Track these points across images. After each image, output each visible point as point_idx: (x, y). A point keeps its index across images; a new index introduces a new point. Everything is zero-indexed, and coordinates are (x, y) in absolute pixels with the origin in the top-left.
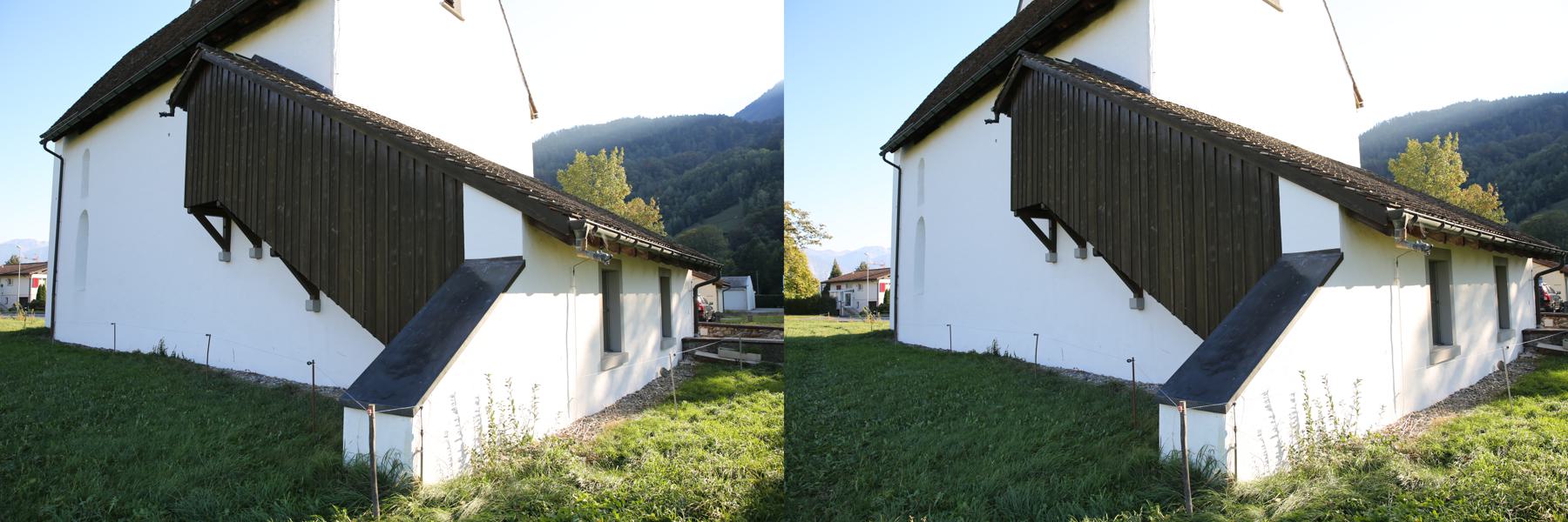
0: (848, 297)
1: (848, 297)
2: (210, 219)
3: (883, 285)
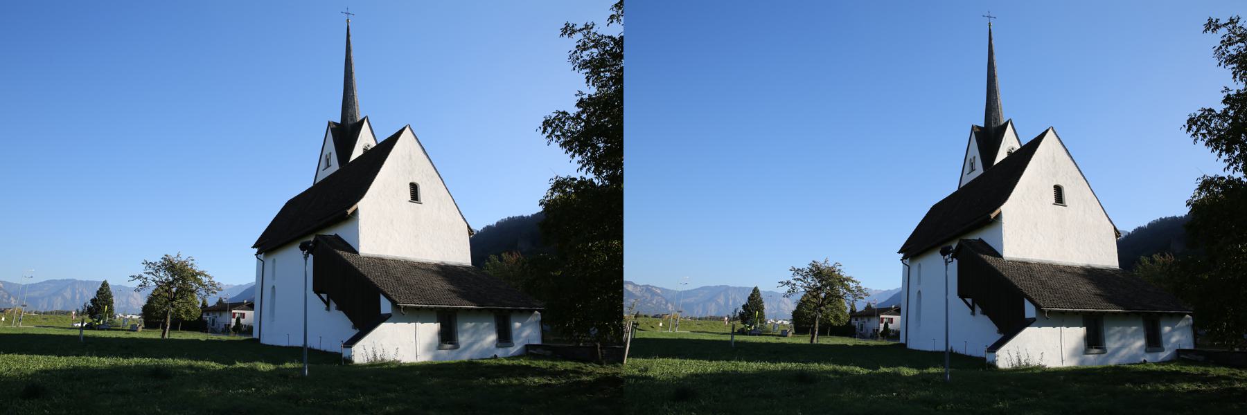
0: (862, 325)
1: (862, 325)
2: (966, 299)
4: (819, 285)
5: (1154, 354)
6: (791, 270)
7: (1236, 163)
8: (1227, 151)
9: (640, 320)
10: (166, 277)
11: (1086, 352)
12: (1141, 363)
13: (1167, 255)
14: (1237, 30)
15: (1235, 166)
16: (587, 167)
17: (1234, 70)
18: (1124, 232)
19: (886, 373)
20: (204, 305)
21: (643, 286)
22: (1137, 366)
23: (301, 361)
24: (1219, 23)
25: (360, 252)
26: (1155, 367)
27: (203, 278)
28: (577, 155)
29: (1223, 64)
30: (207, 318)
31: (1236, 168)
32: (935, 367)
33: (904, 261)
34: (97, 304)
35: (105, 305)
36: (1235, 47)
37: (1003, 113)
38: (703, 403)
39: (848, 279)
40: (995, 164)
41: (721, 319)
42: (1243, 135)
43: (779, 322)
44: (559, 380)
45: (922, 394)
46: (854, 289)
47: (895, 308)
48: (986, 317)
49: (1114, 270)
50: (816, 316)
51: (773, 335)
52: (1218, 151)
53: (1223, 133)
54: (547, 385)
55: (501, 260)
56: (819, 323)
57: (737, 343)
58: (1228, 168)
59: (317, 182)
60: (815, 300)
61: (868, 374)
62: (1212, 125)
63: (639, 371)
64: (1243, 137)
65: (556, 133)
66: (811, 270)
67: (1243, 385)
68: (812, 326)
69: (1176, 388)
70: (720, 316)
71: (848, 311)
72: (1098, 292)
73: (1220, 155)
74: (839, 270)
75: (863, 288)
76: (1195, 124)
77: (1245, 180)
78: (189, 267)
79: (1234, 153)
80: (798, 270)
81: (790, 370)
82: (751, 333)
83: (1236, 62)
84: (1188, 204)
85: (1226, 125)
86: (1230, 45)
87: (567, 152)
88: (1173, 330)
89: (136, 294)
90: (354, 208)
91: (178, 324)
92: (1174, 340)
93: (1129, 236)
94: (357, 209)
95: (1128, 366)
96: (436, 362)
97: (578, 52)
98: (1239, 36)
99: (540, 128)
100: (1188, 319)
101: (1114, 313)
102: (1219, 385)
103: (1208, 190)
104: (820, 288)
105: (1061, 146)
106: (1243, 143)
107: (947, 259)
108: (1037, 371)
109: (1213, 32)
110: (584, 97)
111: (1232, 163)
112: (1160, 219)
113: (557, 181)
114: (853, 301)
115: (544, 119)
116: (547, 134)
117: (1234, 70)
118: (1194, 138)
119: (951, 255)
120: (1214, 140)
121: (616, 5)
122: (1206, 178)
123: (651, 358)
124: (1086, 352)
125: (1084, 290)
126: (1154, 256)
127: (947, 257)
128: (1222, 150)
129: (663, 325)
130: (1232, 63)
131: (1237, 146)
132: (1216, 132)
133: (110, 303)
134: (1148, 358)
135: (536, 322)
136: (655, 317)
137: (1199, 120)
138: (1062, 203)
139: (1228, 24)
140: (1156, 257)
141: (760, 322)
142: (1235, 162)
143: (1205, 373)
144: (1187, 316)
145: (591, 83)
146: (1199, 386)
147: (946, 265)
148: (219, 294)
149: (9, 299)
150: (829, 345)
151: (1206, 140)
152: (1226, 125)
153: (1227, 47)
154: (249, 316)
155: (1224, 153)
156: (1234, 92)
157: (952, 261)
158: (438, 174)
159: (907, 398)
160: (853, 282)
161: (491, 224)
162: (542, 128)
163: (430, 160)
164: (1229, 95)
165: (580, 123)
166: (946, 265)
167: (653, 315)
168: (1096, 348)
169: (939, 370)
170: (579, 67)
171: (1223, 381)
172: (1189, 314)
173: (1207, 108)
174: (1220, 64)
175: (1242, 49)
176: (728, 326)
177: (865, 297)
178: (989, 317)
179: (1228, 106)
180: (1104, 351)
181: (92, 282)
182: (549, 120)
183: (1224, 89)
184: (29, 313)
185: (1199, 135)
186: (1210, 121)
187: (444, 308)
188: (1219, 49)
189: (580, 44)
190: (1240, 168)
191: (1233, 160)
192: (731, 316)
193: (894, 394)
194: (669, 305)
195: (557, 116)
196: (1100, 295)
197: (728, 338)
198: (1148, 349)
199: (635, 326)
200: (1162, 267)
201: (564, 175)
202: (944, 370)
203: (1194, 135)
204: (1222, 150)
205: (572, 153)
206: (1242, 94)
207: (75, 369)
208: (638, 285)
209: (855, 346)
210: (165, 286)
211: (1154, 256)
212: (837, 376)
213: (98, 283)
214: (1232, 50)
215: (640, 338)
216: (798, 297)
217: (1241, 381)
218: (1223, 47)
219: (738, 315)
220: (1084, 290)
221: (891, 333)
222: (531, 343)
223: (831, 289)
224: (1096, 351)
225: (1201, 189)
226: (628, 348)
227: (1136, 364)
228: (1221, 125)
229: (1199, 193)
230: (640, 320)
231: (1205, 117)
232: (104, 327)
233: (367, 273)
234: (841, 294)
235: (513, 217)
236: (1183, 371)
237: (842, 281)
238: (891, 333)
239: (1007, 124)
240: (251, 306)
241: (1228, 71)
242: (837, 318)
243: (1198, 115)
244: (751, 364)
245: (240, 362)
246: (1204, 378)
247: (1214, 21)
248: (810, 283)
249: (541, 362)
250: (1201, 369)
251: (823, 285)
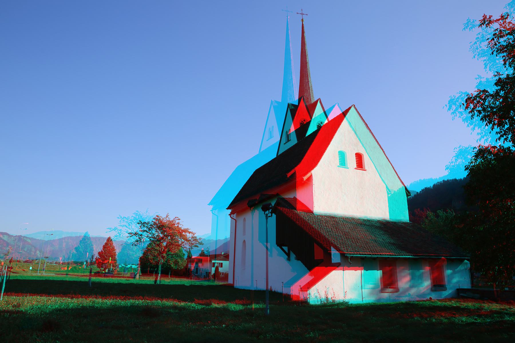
2: (283, 247)
3: (214, 263)
4: (161, 235)
5: (438, 293)
6: (139, 223)
7: (506, 135)
8: (499, 125)
9: (13, 264)
10: (157, 234)
11: (382, 291)
12: (428, 300)
13: (449, 211)
14: (507, 25)
15: (505, 137)
16: (485, 138)
17: (504, 58)
18: (413, 191)
19: (216, 308)
20: (189, 257)
21: (16, 236)
22: (424, 302)
23: (264, 302)
24: (492, 19)
25: (314, 212)
26: (439, 303)
27: (188, 234)
28: (476, 128)
29: (495, 53)
30: (192, 267)
31: (506, 139)
32: (257, 303)
33: (232, 215)
34: (103, 256)
35: (109, 257)
36: (505, 38)
37: (314, 93)
38: (66, 333)
39: (186, 231)
40: (307, 135)
41: (82, 263)
42: (512, 111)
43: (129, 266)
44: (484, 319)
45: (247, 325)
46: (190, 239)
47: (224, 254)
48: (300, 262)
49: (405, 223)
50: (159, 261)
51: (123, 277)
52: (491, 125)
53: (495, 110)
54: (473, 323)
55: (437, 216)
56: (162, 267)
57: (94, 283)
58: (499, 139)
59: (279, 154)
60: (158, 248)
61: (202, 309)
62: (486, 104)
63: (13, 307)
64: (512, 113)
65: (477, 109)
66: (155, 223)
67: (511, 318)
68: (156, 269)
69: (457, 320)
70: (80, 261)
71: (186, 257)
72: (392, 241)
73: (493, 128)
74: (178, 223)
75: (198, 238)
76: (472, 102)
77: (513, 149)
78: (176, 226)
79: (504, 127)
80: (145, 223)
81: (138, 306)
82: (105, 275)
83: (506, 51)
84: (466, 169)
85: (498, 103)
86: (501, 37)
87: (468, 125)
88: (454, 273)
89: (135, 248)
90: (308, 175)
91: (167, 271)
92: (455, 280)
93: (418, 195)
94: (311, 176)
95: (416, 303)
96: (379, 303)
97: (478, 43)
98: (508, 29)
99: (446, 105)
100: (467, 264)
101: (453, 257)
102: (492, 318)
103: (483, 157)
104: (162, 238)
105: (361, 121)
106: (512, 118)
107: (267, 215)
108: (342, 307)
109: (487, 26)
110: (483, 80)
111: (502, 135)
112: (443, 181)
113: (479, 149)
114: (189, 249)
115: (449, 99)
116: (451, 111)
117: (504, 58)
118: (471, 114)
119: (270, 211)
120: (488, 116)
121: (509, 4)
122: (481, 147)
123: (23, 296)
124: (382, 291)
125: (381, 240)
126: (438, 211)
127: (267, 212)
128: (494, 124)
129: (32, 268)
130: (503, 52)
131: (507, 121)
132: (489, 109)
133: (113, 256)
134: (434, 296)
135: (466, 269)
136: (26, 262)
137: (458, 101)
138: (362, 168)
139: (499, 20)
140: (440, 213)
141: (113, 266)
142: (505, 134)
143: (480, 309)
144: (466, 261)
145: (488, 69)
146: (476, 319)
147: (267, 219)
148: (201, 248)
149: (35, 252)
150: (170, 285)
151: (481, 115)
152: (498, 103)
153: (498, 38)
154: (226, 266)
155: (496, 127)
156: (505, 76)
157: (272, 216)
158: (380, 145)
159: (234, 329)
160: (189, 233)
161: (428, 186)
162: (448, 105)
163: (372, 133)
164: (500, 79)
165: (499, 100)
166: (267, 219)
167: (24, 260)
168: (390, 288)
169: (261, 306)
170: (478, 55)
171: (495, 315)
172: (467, 260)
173: (482, 89)
174: (493, 53)
175: (511, 41)
176: (86, 269)
177: (199, 246)
178: (302, 262)
179: (499, 87)
180: (397, 290)
181: (100, 238)
182: (454, 99)
183: (496, 74)
184: (51, 263)
185: (475, 111)
186: (484, 100)
187: (385, 258)
188: (492, 40)
189: (479, 36)
190: (509, 139)
191: (503, 132)
192: (89, 261)
193: (224, 325)
194: (38, 252)
195: (461, 96)
196: (394, 244)
197: (86, 279)
198: (433, 289)
199: (9, 269)
200: (445, 220)
201: (485, 144)
202: (264, 306)
203: (471, 112)
204: (494, 124)
205: (472, 126)
206: (511, 78)
207: (84, 308)
208: (12, 236)
209: (191, 286)
210: (156, 241)
211: (438, 211)
212: (177, 311)
213: (104, 238)
214: (503, 41)
215: (14, 280)
216: (145, 245)
217: (510, 315)
218: (495, 39)
219: (94, 260)
220: (381, 240)
221: (221, 276)
222: (461, 287)
223: (172, 239)
224: (390, 290)
225: (477, 156)
226: (4, 287)
227: (424, 301)
228: (493, 104)
229: (475, 159)
230: (13, 264)
231: (480, 97)
232: (109, 275)
233: (320, 228)
234: (180, 243)
235: (448, 180)
236: (462, 307)
237: (181, 232)
238: (221, 276)
239: (316, 102)
240: (226, 257)
241: (499, 60)
242: (176, 263)
243: (457, 97)
244: (105, 301)
245: (215, 303)
246: (478, 312)
247: (488, 17)
248: (154, 234)
249: (470, 304)
250: (477, 305)
251: (164, 236)
